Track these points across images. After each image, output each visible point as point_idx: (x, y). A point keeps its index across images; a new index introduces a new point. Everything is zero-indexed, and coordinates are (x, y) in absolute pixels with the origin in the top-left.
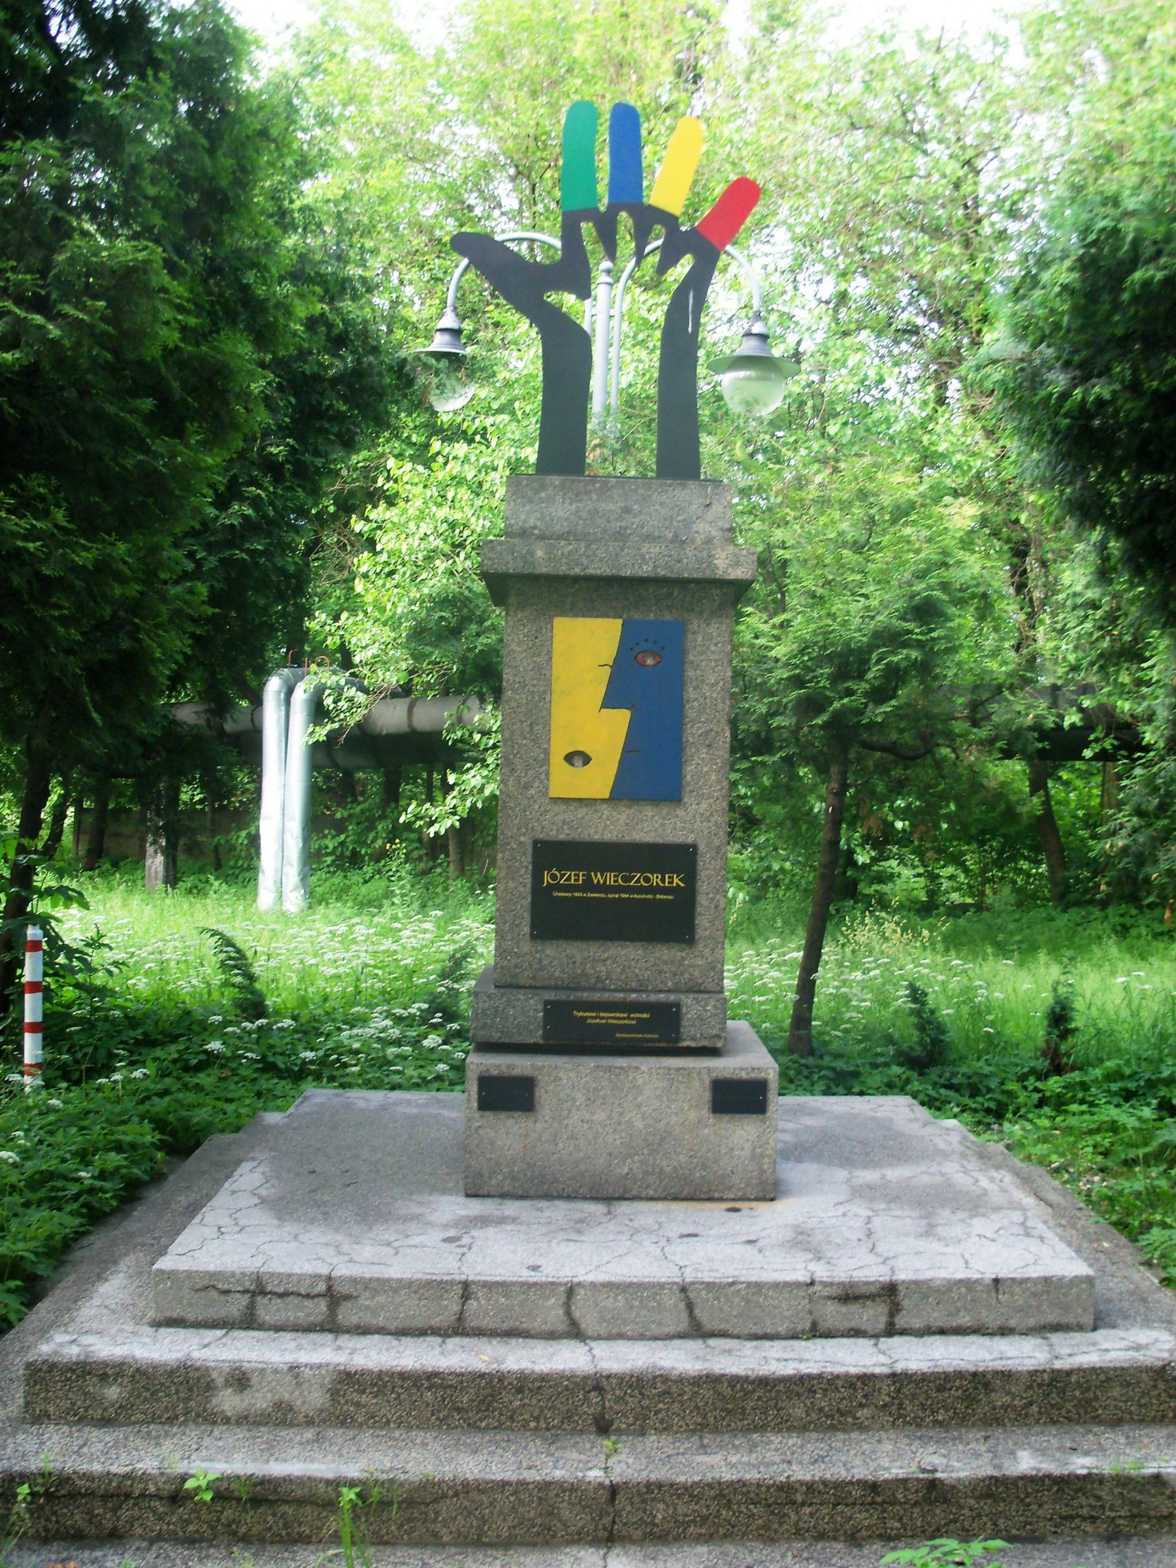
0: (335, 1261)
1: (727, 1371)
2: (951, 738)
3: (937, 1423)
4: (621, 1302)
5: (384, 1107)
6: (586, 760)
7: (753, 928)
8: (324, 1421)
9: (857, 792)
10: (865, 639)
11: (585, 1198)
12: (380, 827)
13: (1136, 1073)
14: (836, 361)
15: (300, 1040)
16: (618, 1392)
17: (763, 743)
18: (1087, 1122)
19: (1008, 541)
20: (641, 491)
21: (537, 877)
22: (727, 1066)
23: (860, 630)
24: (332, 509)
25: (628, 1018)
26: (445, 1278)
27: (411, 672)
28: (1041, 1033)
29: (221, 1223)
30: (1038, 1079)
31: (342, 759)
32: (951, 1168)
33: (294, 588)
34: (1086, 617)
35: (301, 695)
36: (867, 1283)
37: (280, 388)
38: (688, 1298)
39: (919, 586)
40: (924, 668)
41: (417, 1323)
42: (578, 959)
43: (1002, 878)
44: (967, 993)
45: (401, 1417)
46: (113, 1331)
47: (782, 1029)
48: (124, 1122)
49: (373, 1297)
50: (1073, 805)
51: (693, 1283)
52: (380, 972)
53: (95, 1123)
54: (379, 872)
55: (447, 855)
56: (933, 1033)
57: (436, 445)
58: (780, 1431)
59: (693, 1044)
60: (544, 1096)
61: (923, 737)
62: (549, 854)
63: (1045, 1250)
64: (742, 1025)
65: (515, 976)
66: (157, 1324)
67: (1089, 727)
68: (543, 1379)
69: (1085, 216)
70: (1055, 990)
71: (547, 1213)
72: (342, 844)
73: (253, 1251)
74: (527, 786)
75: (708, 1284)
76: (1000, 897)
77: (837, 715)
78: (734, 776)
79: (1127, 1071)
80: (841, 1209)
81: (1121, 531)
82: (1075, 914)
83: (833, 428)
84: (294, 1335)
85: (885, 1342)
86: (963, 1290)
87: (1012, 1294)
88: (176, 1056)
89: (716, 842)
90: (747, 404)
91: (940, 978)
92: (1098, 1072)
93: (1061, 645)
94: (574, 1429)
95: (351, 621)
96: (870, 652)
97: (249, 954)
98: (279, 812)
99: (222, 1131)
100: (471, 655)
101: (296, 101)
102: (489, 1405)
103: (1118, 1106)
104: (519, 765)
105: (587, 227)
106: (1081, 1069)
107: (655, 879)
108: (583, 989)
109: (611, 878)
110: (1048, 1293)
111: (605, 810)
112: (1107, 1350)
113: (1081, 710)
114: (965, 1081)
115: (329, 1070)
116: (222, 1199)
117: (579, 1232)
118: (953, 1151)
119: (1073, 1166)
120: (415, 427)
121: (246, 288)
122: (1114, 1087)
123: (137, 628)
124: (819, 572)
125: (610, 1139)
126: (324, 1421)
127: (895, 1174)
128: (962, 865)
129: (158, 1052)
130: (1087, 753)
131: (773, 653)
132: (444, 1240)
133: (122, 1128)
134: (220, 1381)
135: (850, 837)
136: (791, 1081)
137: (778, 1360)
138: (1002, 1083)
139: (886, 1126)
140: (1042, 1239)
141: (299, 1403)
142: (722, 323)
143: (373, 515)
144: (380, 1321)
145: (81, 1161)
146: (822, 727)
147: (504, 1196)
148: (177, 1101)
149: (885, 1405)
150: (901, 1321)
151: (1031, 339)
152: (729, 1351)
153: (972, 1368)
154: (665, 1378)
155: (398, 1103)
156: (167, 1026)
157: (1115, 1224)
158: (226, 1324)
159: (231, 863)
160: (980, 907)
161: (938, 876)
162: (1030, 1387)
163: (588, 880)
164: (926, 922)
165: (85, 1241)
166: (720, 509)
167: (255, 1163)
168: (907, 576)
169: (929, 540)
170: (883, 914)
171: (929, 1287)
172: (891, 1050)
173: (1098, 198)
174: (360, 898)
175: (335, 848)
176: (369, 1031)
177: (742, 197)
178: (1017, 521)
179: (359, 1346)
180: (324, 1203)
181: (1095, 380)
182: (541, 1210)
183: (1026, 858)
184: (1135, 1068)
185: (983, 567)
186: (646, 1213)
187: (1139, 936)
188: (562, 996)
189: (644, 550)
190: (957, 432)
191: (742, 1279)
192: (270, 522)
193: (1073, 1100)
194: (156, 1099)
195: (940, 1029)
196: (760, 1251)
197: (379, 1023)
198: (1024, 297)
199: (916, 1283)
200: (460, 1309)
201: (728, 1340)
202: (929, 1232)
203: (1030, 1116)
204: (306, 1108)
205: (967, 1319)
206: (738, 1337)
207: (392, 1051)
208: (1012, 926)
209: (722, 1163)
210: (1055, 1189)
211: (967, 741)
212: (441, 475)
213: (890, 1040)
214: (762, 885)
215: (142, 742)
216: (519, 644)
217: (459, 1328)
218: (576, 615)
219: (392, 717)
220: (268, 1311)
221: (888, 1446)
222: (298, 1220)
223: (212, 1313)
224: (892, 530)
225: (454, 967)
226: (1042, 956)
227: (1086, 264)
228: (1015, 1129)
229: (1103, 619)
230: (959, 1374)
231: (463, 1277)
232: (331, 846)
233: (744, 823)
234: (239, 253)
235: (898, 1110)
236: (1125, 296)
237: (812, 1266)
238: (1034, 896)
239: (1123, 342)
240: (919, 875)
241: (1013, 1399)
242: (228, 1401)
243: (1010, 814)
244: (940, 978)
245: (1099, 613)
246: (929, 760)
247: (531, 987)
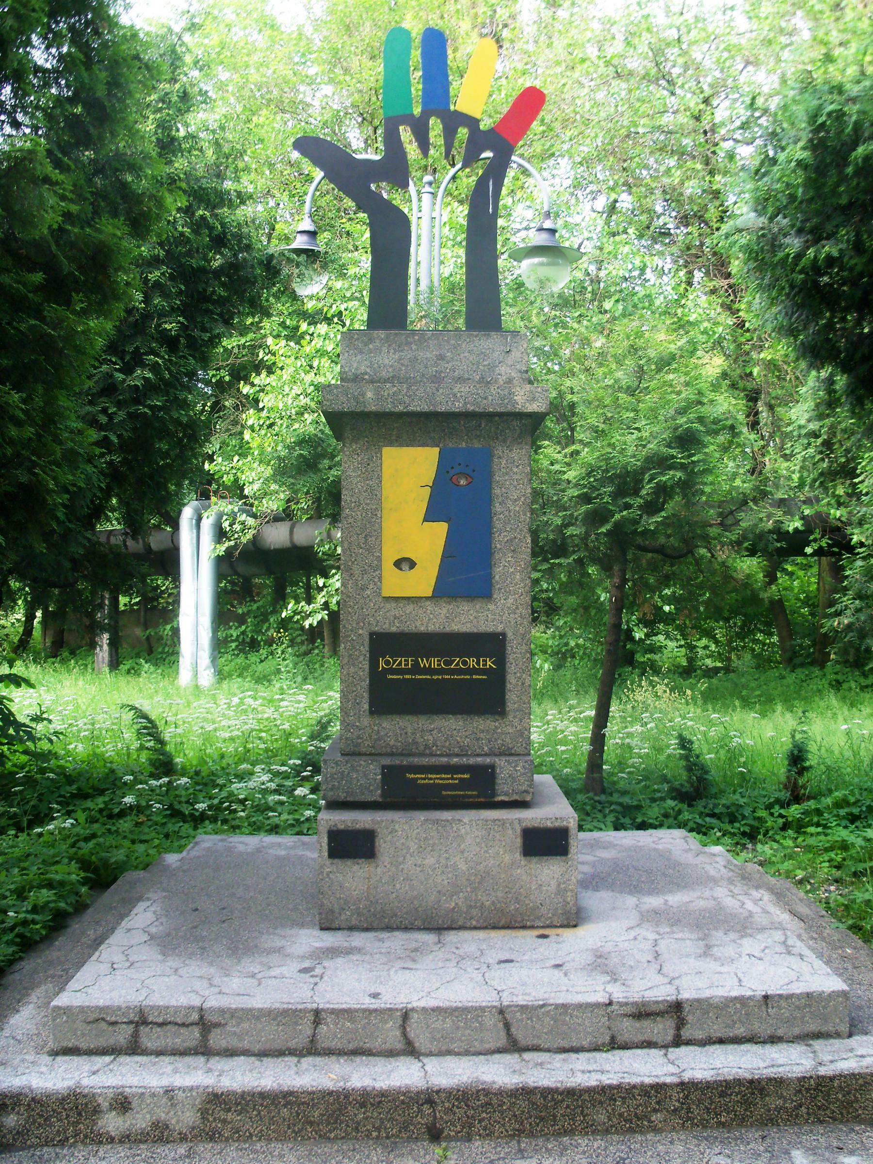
0: (207, 993)
1: (540, 1084)
2: (706, 540)
3: (723, 1125)
4: (448, 1023)
5: (258, 850)
6: (412, 564)
7: (554, 692)
8: (196, 1137)
9: (634, 585)
10: (639, 463)
11: (419, 929)
12: (272, 620)
13: (859, 801)
14: (609, 253)
15: (201, 791)
16: (447, 1105)
17: (560, 549)
18: (821, 841)
19: (744, 390)
20: (453, 342)
21: (374, 664)
22: (533, 817)
23: (634, 456)
24: (227, 378)
25: (452, 778)
26: (300, 1007)
27: (288, 501)
28: (783, 770)
29: (115, 959)
30: (782, 807)
31: (242, 569)
32: (721, 892)
33: (193, 435)
34: (809, 444)
35: (207, 523)
36: (657, 1002)
37: (172, 278)
38: (505, 1018)
39: (681, 420)
40: (687, 486)
41: (277, 1045)
42: (409, 730)
43: (744, 647)
44: (723, 741)
45: (262, 1130)
46: (16, 1062)
47: (579, 772)
48: (57, 863)
49: (238, 1024)
50: (796, 591)
51: (509, 1006)
52: (264, 734)
53: (33, 864)
54: (272, 653)
55: (323, 640)
56: (698, 773)
57: (304, 326)
58: (587, 1134)
59: (506, 799)
60: (383, 845)
61: (685, 541)
62: (383, 644)
63: (805, 967)
64: (547, 778)
65: (357, 745)
66: (55, 1053)
67: (809, 531)
68: (383, 1095)
69: (815, 103)
70: (793, 737)
71: (387, 944)
72: (243, 633)
73: (139, 985)
74: (364, 588)
75: (522, 1007)
76: (744, 662)
77: (617, 525)
78: (536, 575)
79: (852, 799)
80: (633, 934)
81: (846, 368)
82: (801, 673)
83: (608, 305)
84: (172, 1058)
85: (674, 1053)
86: (738, 1006)
87: (779, 1007)
88: (102, 806)
89: (522, 630)
90: (541, 282)
91: (702, 728)
92: (829, 801)
93: (789, 468)
94: (410, 1137)
95: (241, 462)
96: (643, 474)
97: (160, 724)
98: (193, 610)
99: (136, 868)
100: (325, 485)
101: (179, 49)
102: (337, 1119)
103: (846, 827)
105: (406, 134)
106: (814, 798)
107: (472, 662)
108: (413, 755)
109: (435, 663)
110: (810, 1006)
111: (429, 606)
112: (862, 1056)
113: (803, 518)
114: (724, 810)
115: (221, 817)
116: (118, 938)
117: (414, 960)
118: (722, 878)
119: (813, 877)
120: (290, 314)
121: (124, 185)
122: (842, 812)
123: (35, 465)
124: (600, 411)
125: (439, 880)
126: (196, 1137)
127: (676, 899)
128: (713, 638)
129: (89, 804)
130: (809, 550)
131: (566, 477)
132: (300, 971)
133: (53, 868)
134: (105, 1105)
135: (630, 619)
136: (588, 814)
137: (583, 1072)
138: (754, 812)
139: (665, 856)
140: (801, 956)
141: (173, 1121)
142: (519, 219)
143: (257, 381)
144: (245, 1044)
145: (18, 897)
146: (605, 534)
147: (351, 929)
148: (99, 844)
149: (675, 1110)
150: (686, 1033)
151: (770, 210)
152: (541, 1064)
153: (748, 1076)
154: (487, 1092)
155: (273, 845)
156: (96, 782)
157: (851, 928)
158: (114, 1051)
159: (160, 650)
160: (727, 670)
161: (696, 647)
162: (800, 1091)
163: (416, 664)
164: (688, 682)
165: (17, 967)
166: (518, 355)
167: (148, 903)
168: (672, 412)
169: (687, 384)
170: (656, 679)
171: (710, 1005)
172: (666, 787)
173: (826, 87)
174: (257, 674)
175: (238, 636)
176: (251, 784)
177: (530, 102)
178: (751, 373)
179: (226, 1068)
180: (203, 938)
181: (823, 242)
182: (382, 940)
183: (761, 631)
184: (858, 796)
185: (727, 405)
186: (469, 942)
187: (850, 689)
188: (397, 761)
189: (456, 390)
190: (702, 305)
191: (551, 1001)
192: (167, 384)
193: (810, 824)
194: (82, 844)
195: (704, 770)
196: (566, 974)
197: (261, 778)
198: (764, 175)
199: (698, 1001)
200: (312, 1033)
201: (540, 1054)
202: (707, 952)
203: (777, 837)
204: (193, 853)
205: (742, 1030)
206: (548, 1050)
207: (273, 798)
208: (753, 684)
209: (532, 897)
210: (801, 900)
211: (720, 542)
212: (308, 349)
213: (665, 779)
214: (562, 657)
215: (73, 561)
216: (354, 470)
217: (312, 1049)
218: (401, 445)
219: (277, 536)
220: (150, 1038)
221: (679, 1148)
222: (179, 955)
223: (101, 1042)
224: (658, 377)
225: (320, 731)
226: (779, 708)
227: (816, 146)
228: (766, 849)
229: (823, 444)
230: (738, 1082)
231: (315, 1006)
232: (235, 635)
233: (544, 610)
234: (118, 155)
235: (673, 841)
236: (850, 170)
237: (610, 988)
238: (769, 660)
239: (846, 210)
240: (681, 646)
241: (785, 1102)
242: (112, 1123)
243: (755, 599)
244: (702, 728)
245: (819, 441)
246: (690, 559)
247: (371, 754)
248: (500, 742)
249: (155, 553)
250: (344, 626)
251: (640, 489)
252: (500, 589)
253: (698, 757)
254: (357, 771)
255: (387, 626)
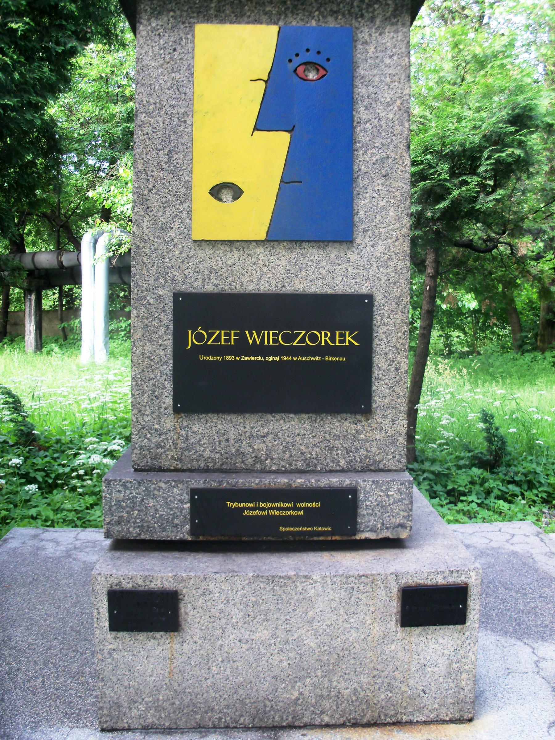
6: (237, 192)
21: (179, 339)
25: (295, 508)
42: (232, 436)
60: (190, 612)
62: (193, 310)
65: (156, 457)
74: (165, 228)
77: (456, 203)
82: (528, 357)
96: (481, 152)
104: (155, 201)
107: (324, 337)
109: (269, 337)
111: (261, 253)
114: (523, 478)
125: (275, 661)
159: (72, 337)
161: (450, 336)
163: (242, 339)
175: (126, 327)
183: (497, 326)
188: (212, 482)
216: (154, 58)
218: (223, 21)
232: (124, 326)
247: (176, 470)
248: (363, 452)
249: (66, 268)
250: (137, 285)
251: (478, 167)
252: (365, 231)
253: (497, 429)
254: (155, 497)
255: (199, 283)
